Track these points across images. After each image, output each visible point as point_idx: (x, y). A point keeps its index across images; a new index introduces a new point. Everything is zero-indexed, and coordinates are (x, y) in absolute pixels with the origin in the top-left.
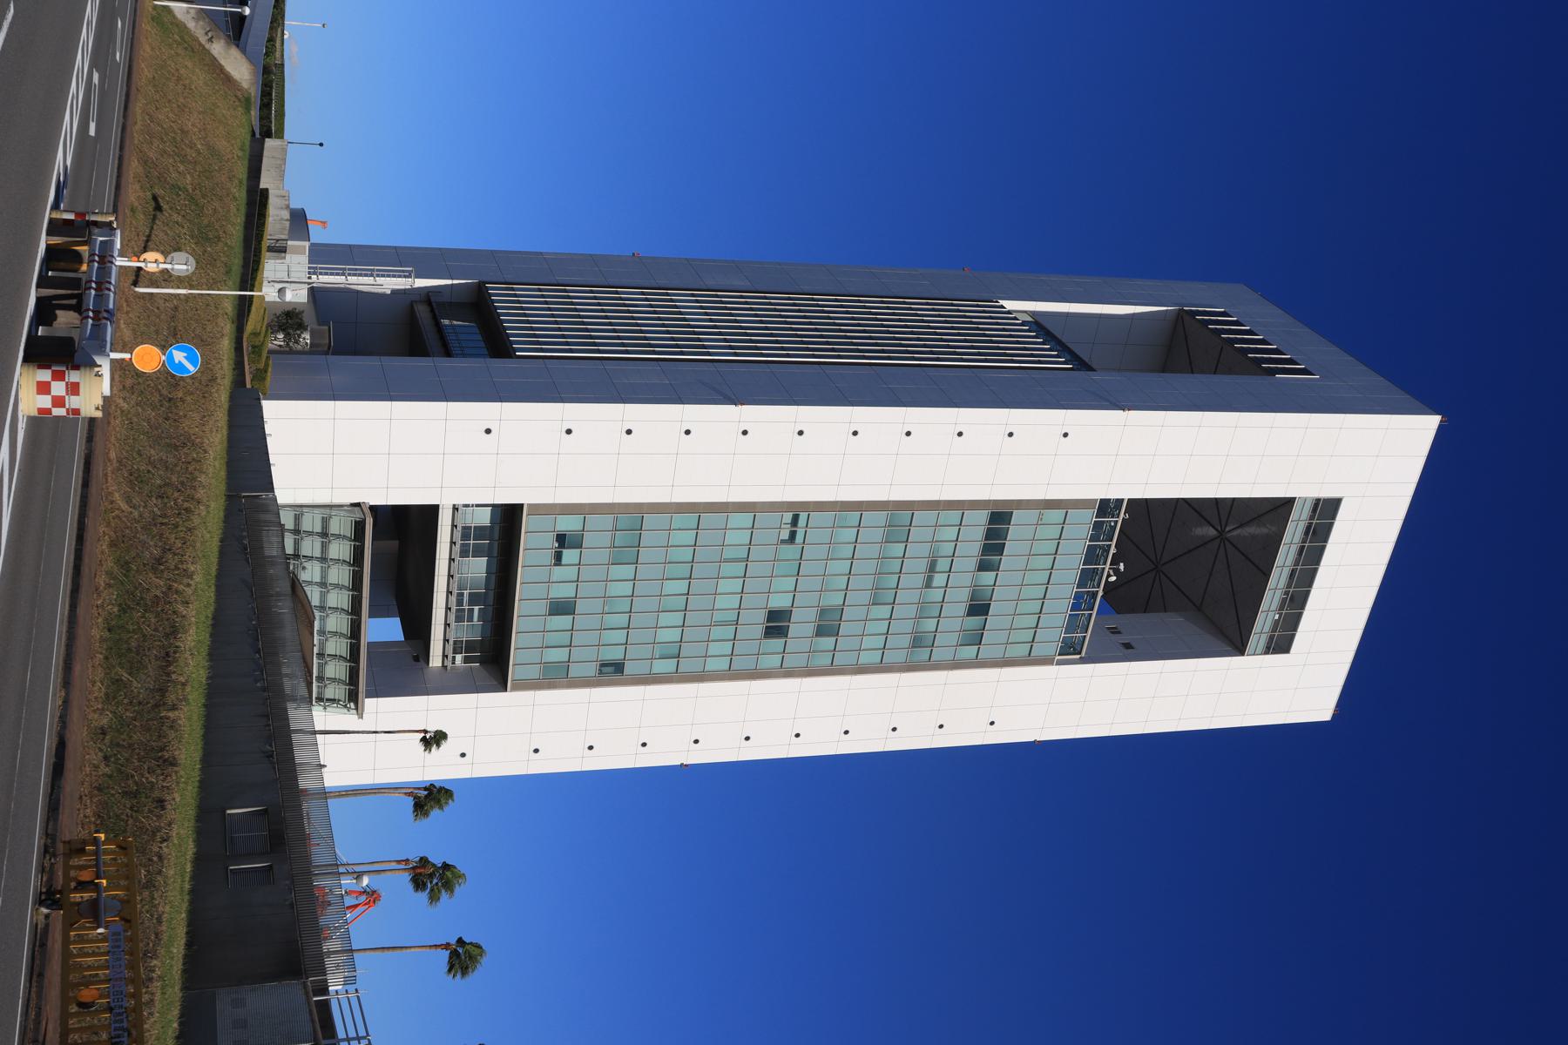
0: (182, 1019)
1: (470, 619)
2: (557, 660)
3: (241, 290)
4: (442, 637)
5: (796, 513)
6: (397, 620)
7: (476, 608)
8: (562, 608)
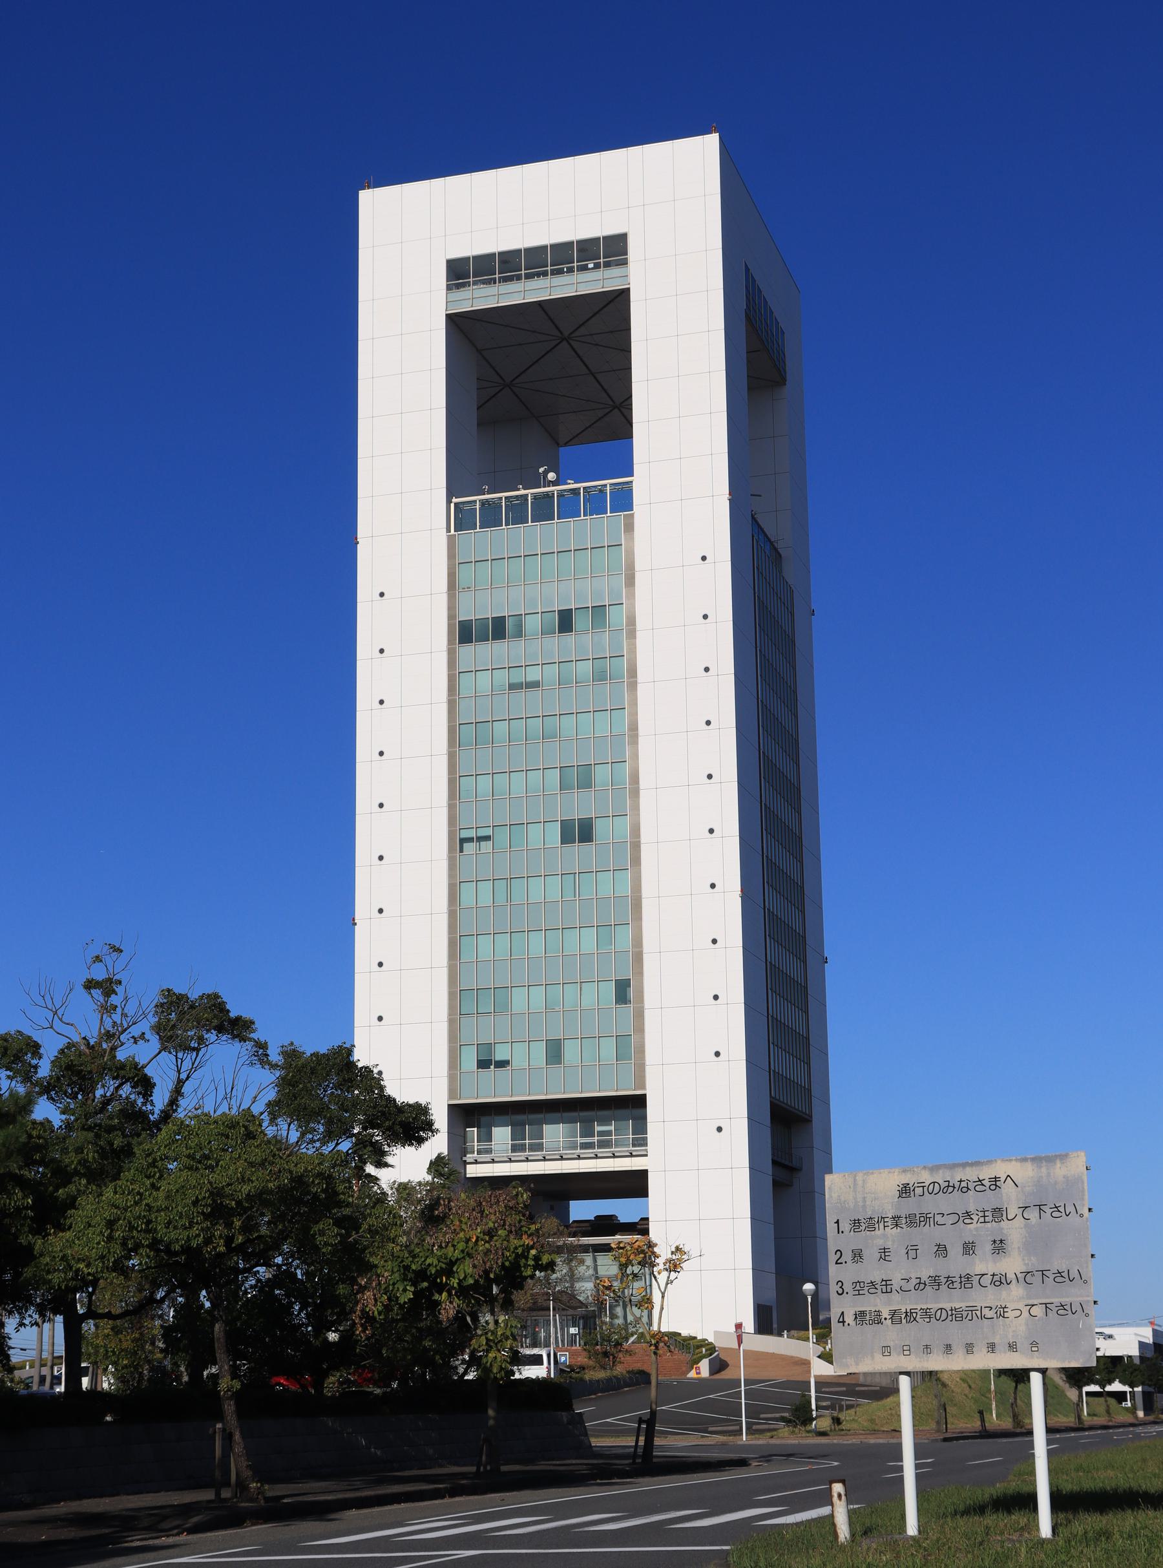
0: (614, 1380)
1: (609, 1133)
2: (810, 1028)
3: (744, 1380)
4: (525, 1164)
5: (459, 843)
6: (570, 1202)
7: (598, 1128)
8: (555, 1052)
